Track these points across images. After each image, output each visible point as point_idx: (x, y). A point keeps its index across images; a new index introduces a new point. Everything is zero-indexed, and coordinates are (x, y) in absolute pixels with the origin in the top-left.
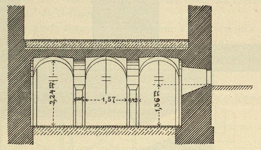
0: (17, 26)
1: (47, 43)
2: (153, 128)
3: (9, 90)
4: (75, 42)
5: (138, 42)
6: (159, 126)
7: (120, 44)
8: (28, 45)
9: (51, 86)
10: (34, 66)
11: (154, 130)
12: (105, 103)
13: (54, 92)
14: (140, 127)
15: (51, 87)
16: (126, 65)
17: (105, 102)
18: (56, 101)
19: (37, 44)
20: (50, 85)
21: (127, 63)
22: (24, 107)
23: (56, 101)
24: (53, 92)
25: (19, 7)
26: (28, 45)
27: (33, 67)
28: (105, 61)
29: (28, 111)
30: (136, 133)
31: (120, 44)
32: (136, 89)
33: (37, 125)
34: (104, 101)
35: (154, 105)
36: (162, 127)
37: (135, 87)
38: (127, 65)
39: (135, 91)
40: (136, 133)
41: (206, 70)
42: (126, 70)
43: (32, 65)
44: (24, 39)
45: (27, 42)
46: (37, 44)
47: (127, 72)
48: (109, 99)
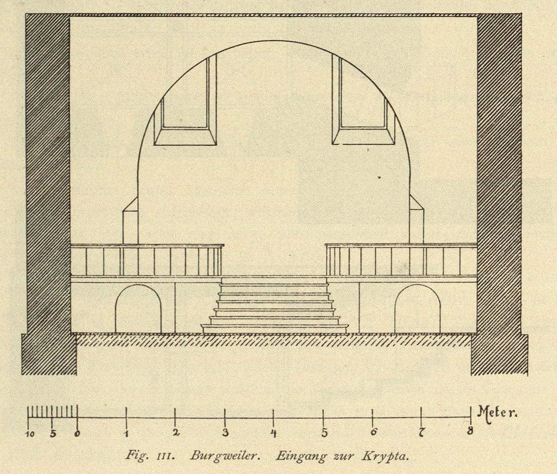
0: (489, 184)
1: (361, 339)
2: (333, 337)
4: (332, 336)
5: (431, 337)
6: (177, 334)
8: (80, 342)
11: (335, 340)
13: (273, 436)
14: (88, 334)
18: (223, 435)
23: (223, 435)
24: (273, 434)
26: (80, 342)
30: (425, 343)
33: (116, 330)
36: (165, 334)
40: (425, 343)
41: (176, 332)
44: (70, 273)
45: (78, 337)
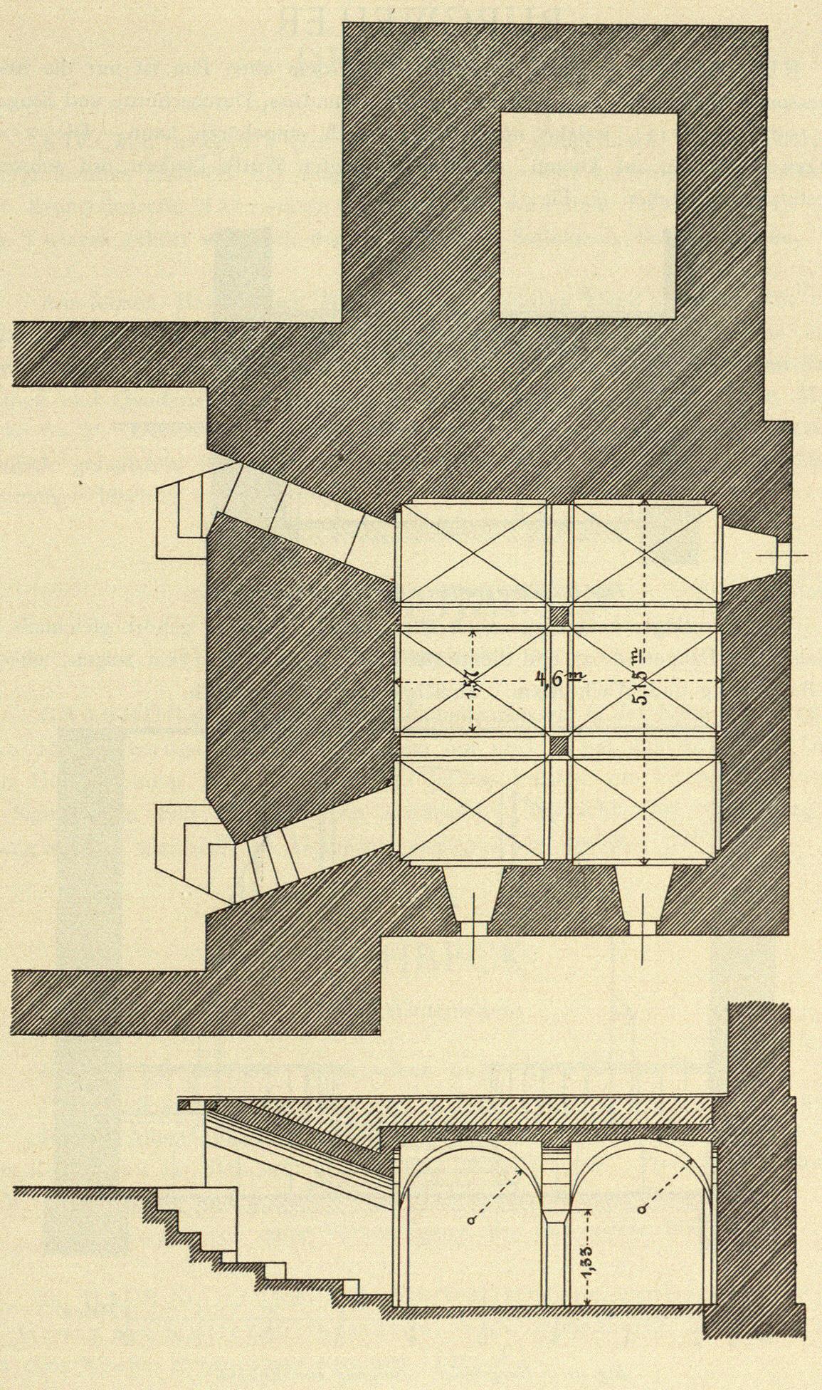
3: (783, 854)
7: (535, 1114)
9: (635, 659)
10: (401, 1183)
12: (593, 1271)
15: (636, 662)
16: (540, 1159)
17: (592, 1271)
19: (303, 1116)
20: (634, 657)
21: (542, 1153)
22: (218, 788)
25: (769, 1006)
27: (400, 1187)
28: (789, 558)
29: (734, 1055)
31: (535, 1114)
32: (563, 1221)
34: (590, 1274)
35: (579, 1251)
37: (561, 1216)
38: (543, 1159)
39: (562, 1225)
42: (540, 1185)
43: (396, 1164)
46: (303, 1116)
47: (541, 1193)
48: (638, 702)
